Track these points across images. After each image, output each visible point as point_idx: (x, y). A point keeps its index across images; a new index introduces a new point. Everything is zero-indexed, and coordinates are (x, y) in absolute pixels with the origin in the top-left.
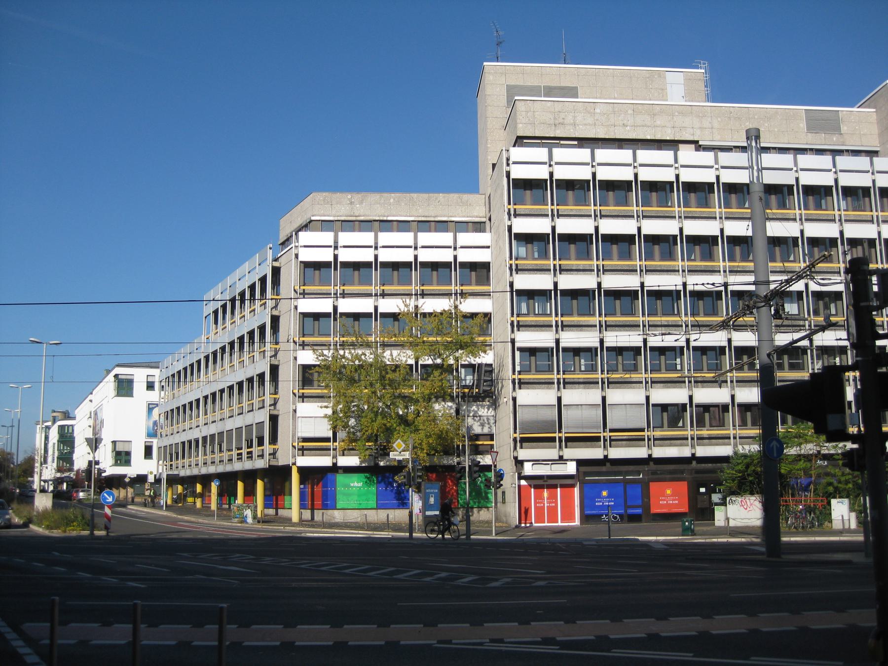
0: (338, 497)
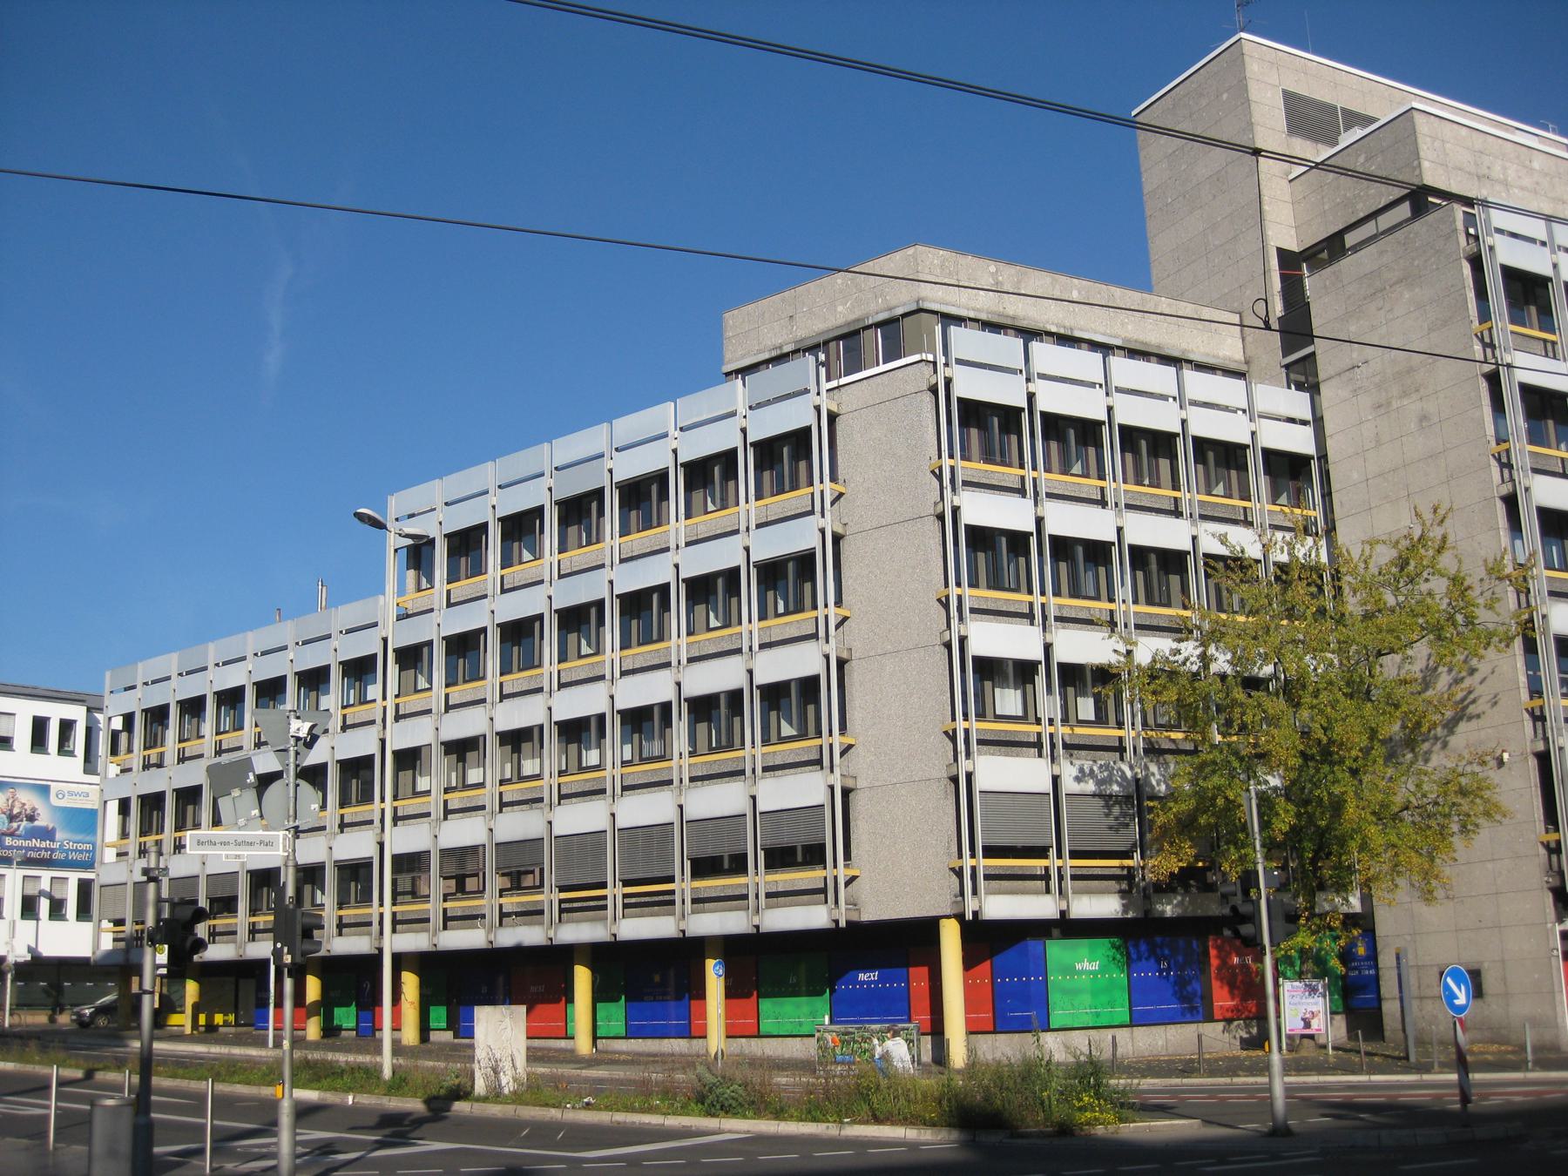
0: (1055, 998)
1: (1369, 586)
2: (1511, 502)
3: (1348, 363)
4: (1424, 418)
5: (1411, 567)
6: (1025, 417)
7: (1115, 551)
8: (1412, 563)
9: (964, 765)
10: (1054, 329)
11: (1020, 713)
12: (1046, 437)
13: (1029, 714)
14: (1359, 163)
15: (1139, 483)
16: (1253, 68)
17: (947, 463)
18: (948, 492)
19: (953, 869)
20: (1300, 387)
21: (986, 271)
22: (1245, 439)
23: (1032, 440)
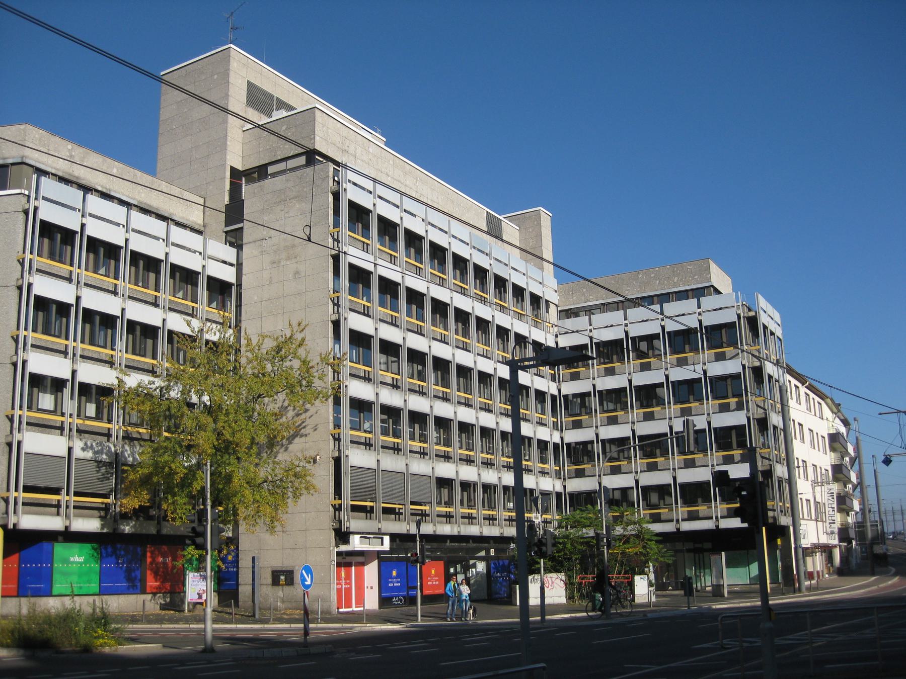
0: (56, 577)
1: (260, 360)
2: (336, 324)
3: (260, 236)
4: (297, 273)
5: (283, 352)
6: (78, 237)
7: (119, 322)
8: (284, 350)
9: (17, 437)
10: (100, 189)
11: (52, 409)
12: (88, 251)
13: (57, 410)
14: (282, 130)
15: (136, 284)
16: (234, 65)
17: (28, 256)
18: (26, 274)
19: (3, 498)
20: (232, 244)
21: (66, 148)
22: (162, 257)
23: (80, 252)
